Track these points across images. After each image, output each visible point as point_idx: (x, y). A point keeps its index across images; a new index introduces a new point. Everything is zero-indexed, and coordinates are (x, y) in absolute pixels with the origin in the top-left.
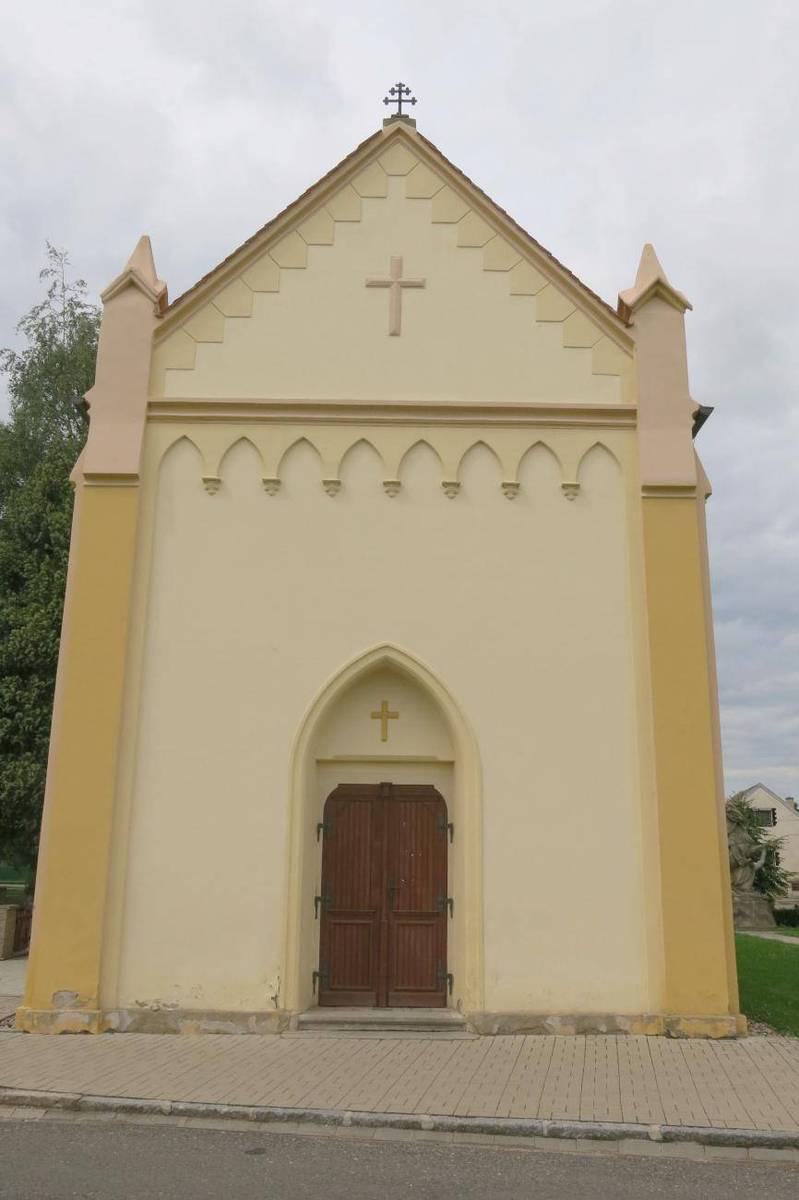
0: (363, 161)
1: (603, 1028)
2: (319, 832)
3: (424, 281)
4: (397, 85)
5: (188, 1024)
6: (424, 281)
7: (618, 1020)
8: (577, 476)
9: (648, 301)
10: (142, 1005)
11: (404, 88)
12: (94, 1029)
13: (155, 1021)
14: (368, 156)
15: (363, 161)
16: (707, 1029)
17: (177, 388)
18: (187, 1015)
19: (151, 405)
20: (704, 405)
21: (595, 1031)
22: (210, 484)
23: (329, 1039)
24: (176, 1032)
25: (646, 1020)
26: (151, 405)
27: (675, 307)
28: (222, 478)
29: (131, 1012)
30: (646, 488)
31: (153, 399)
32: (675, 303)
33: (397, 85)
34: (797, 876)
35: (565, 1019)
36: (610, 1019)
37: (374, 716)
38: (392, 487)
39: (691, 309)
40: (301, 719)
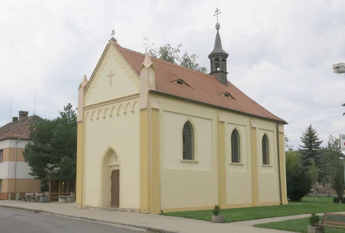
0: (106, 53)
5: (90, 209)
9: (143, 68)
10: (87, 205)
12: (81, 208)
13: (88, 208)
14: (107, 49)
15: (106, 53)
16: (144, 212)
18: (91, 207)
19: (84, 108)
20: (228, 59)
23: (234, 166)
24: (89, 209)
26: (84, 108)
27: (153, 69)
29: (86, 206)
30: (140, 110)
31: (84, 107)
32: (153, 68)
35: (129, 209)
36: (134, 210)
37: (115, 158)
39: (60, 112)
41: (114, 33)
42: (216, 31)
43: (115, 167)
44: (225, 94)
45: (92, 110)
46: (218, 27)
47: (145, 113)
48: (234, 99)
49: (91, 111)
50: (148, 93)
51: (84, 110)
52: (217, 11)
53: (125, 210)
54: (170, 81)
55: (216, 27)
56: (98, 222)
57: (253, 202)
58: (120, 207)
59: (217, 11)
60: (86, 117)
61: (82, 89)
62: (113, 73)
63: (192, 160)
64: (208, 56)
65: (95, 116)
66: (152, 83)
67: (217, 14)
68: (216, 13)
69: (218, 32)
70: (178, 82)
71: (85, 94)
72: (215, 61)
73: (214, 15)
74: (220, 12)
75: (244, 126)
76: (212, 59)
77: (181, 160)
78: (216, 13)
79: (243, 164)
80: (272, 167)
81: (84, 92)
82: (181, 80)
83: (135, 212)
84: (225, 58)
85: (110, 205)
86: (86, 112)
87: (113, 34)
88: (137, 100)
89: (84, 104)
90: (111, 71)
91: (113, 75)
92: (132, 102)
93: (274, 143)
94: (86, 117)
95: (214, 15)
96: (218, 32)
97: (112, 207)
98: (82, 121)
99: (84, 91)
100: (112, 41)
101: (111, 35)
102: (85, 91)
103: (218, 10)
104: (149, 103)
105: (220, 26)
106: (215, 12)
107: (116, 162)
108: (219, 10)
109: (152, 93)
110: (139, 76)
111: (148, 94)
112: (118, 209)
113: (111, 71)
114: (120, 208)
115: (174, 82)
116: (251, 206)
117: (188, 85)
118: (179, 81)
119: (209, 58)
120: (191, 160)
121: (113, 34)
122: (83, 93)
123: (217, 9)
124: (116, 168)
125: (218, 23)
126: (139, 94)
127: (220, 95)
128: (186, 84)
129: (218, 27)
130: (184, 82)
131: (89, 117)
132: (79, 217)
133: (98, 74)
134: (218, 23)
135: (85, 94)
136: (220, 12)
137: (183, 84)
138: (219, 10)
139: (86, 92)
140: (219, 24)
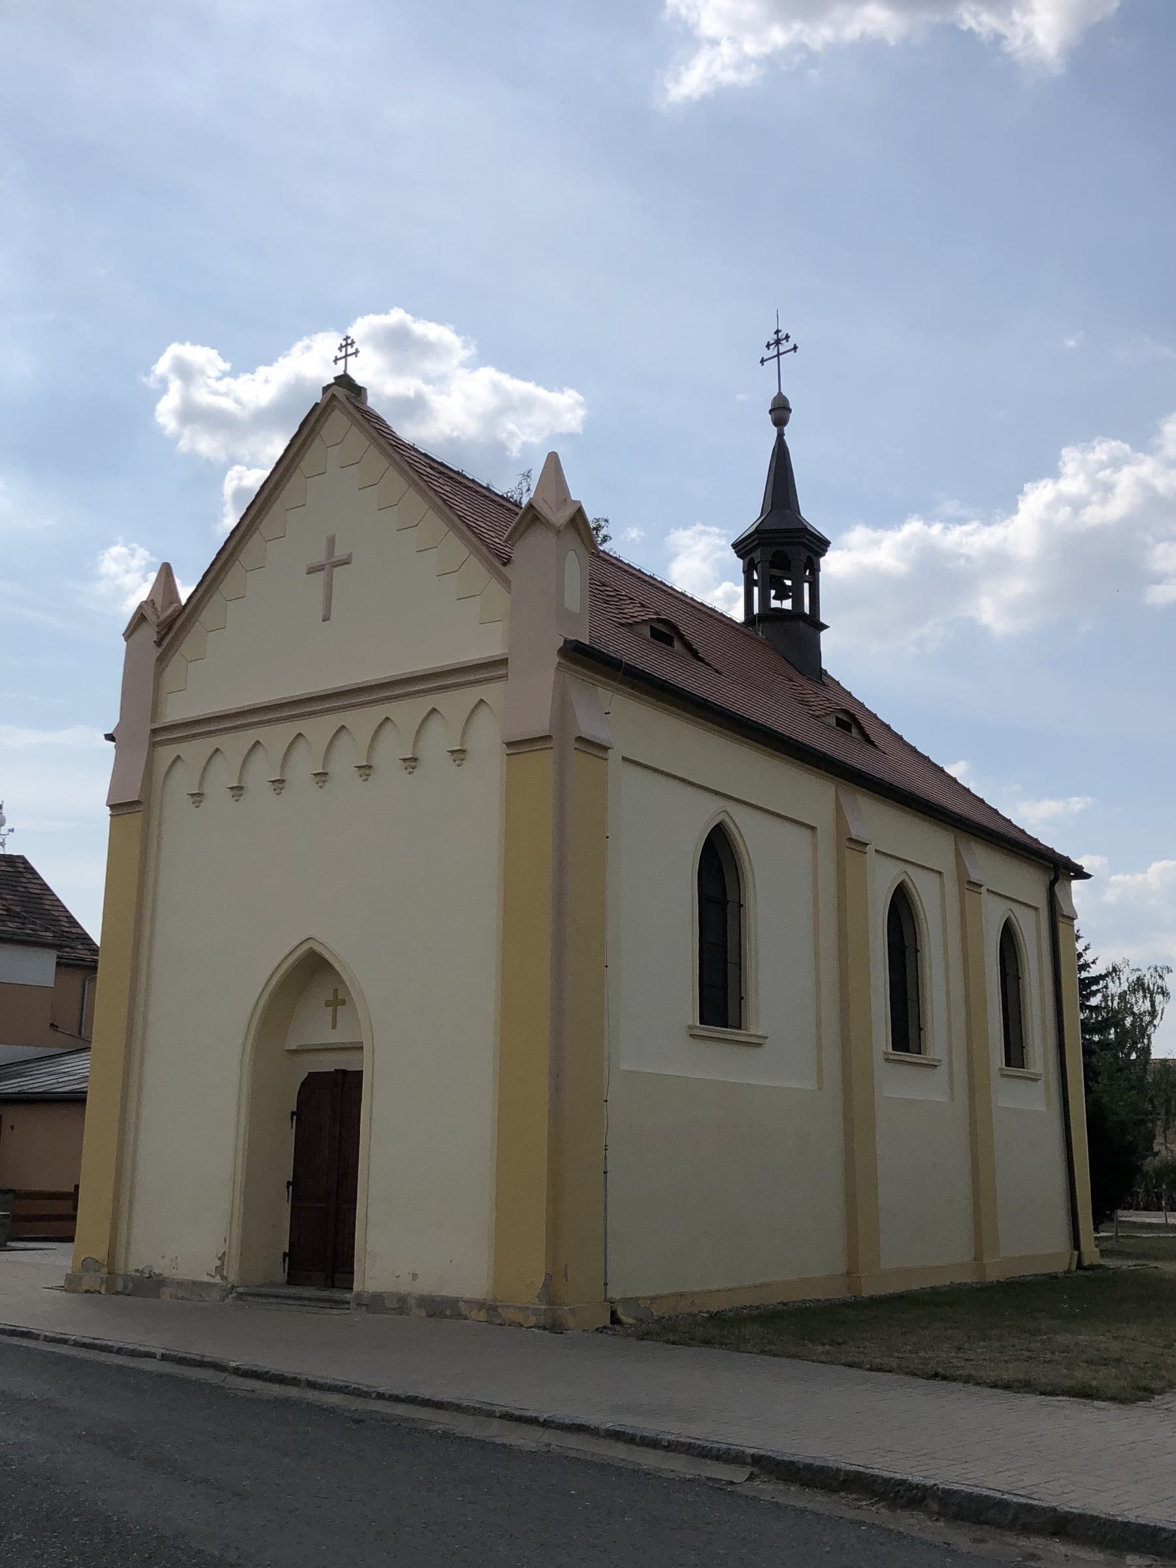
1: (448, 1312)
2: (292, 1120)
3: (350, 555)
4: (352, 340)
6: (350, 555)
7: (462, 1305)
8: (414, 749)
9: (528, 527)
11: (349, 341)
17: (176, 711)
19: (154, 732)
21: (442, 1315)
22: (456, 755)
23: (905, 1070)
25: (481, 1305)
26: (154, 732)
27: (579, 535)
28: (466, 747)
30: (509, 745)
31: (156, 726)
33: (352, 340)
34: (1169, 1268)
36: (454, 1302)
38: (235, 792)
40: (249, 1009)
41: (350, 350)
42: (774, 431)
43: (322, 1056)
44: (837, 718)
45: (204, 746)
46: (780, 412)
47: (543, 763)
48: (872, 743)
49: (195, 751)
50: (557, 659)
51: (154, 745)
52: (778, 342)
53: (375, 1303)
54: (622, 621)
55: (771, 412)
56: (312, 1396)
57: (978, 1258)
58: (357, 1286)
59: (778, 342)
60: (164, 784)
61: (149, 633)
62: (340, 553)
63: (732, 1027)
64: (734, 546)
65: (222, 776)
66: (576, 609)
67: (778, 355)
68: (773, 351)
69: (781, 436)
70: (656, 633)
71: (162, 660)
72: (771, 568)
73: (762, 361)
74: (795, 348)
75: (932, 870)
76: (757, 555)
77: (690, 1027)
78: (773, 351)
79: (935, 1060)
80: (1036, 1080)
81: (160, 650)
82: (665, 622)
83: (460, 1316)
84: (814, 558)
85: (280, 1273)
86: (166, 754)
87: (346, 356)
88: (491, 692)
89: (155, 712)
90: (331, 542)
91: (346, 562)
92: (456, 703)
93: (1040, 963)
94: (164, 784)
95: (762, 361)
96: (781, 436)
97: (292, 1280)
98: (137, 803)
99: (159, 643)
100: (341, 392)
101: (336, 360)
102: (165, 643)
103: (782, 335)
104: (563, 710)
105: (790, 410)
106: (768, 346)
107: (334, 1027)
108: (787, 337)
109: (576, 662)
110: (503, 569)
111: (559, 663)
112: (348, 1296)
113: (331, 542)
114: (359, 1295)
115: (639, 629)
116: (968, 1278)
117: (695, 654)
118: (659, 626)
119: (736, 552)
120: (726, 1027)
121: (346, 356)
122: (156, 652)
123: (777, 332)
124: (328, 1064)
125: (780, 393)
126: (503, 662)
127: (818, 717)
128: (688, 645)
129: (780, 412)
130: (681, 637)
131: (182, 783)
132: (159, 1352)
133: (246, 557)
134: (780, 393)
135: (162, 660)
136: (795, 348)
137: (677, 644)
138: (787, 337)
139: (170, 647)
140: (785, 400)
